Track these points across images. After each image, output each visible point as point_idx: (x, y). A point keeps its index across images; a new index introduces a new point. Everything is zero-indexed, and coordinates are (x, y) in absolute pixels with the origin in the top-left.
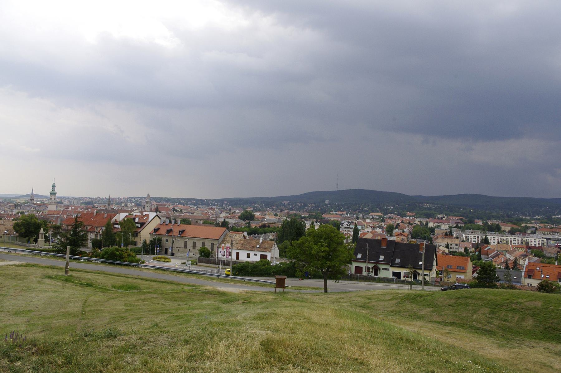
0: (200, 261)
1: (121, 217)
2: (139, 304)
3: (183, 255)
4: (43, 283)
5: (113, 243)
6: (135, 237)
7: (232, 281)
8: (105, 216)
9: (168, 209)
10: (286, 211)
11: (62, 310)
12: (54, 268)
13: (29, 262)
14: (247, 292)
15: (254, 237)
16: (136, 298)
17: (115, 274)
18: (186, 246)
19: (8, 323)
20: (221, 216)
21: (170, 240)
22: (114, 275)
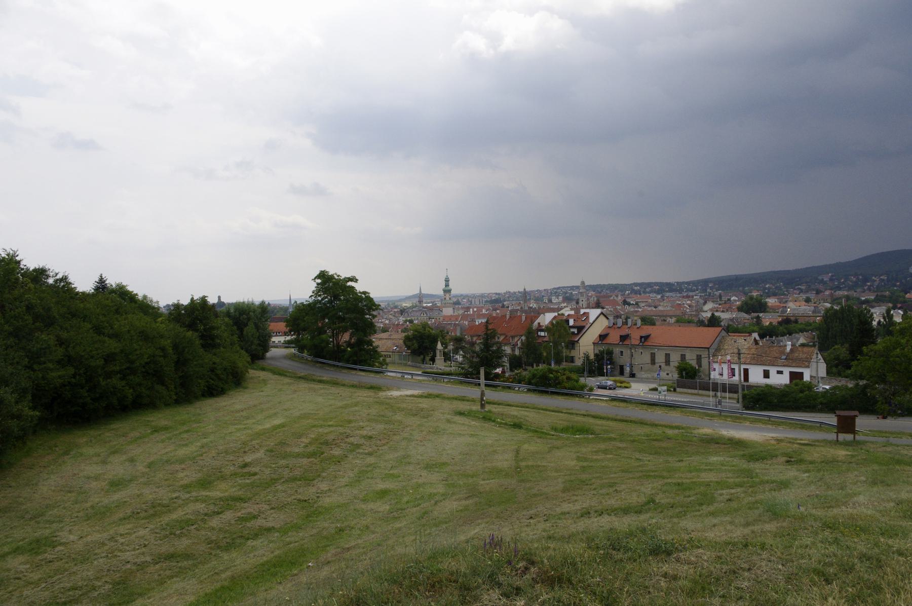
0: (681, 385)
1: (547, 319)
2: (599, 457)
3: (649, 376)
4: (454, 423)
5: (538, 360)
6: (571, 349)
7: (745, 419)
8: (524, 318)
9: (614, 303)
10: (827, 293)
11: (488, 465)
12: (463, 400)
13: (431, 391)
14: (779, 441)
15: (769, 342)
16: (593, 448)
17: (552, 409)
18: (653, 362)
19: (420, 481)
20: (706, 308)
21: (627, 352)
22: (550, 411)
